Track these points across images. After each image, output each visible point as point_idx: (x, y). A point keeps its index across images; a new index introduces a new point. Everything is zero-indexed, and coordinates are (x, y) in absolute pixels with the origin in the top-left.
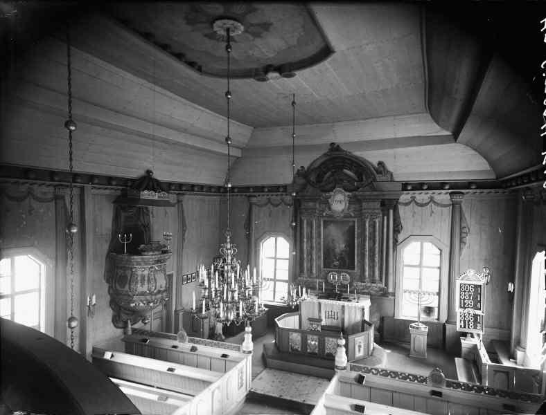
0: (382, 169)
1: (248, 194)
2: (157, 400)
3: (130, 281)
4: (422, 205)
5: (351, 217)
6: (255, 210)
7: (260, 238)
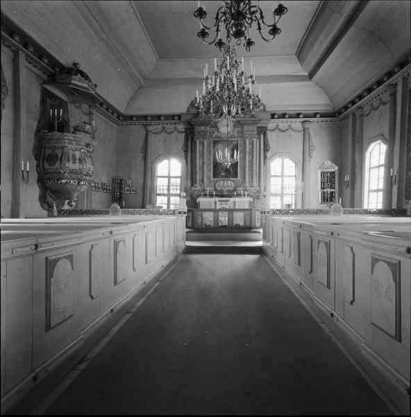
3: (61, 158)
4: (283, 131)
5: (235, 137)
6: (152, 137)
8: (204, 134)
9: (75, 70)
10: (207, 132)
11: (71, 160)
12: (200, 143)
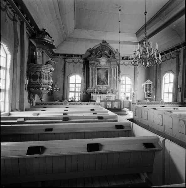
0: (117, 52)
3: (40, 77)
5: (107, 67)
6: (67, 64)
7: (164, 74)
9: (44, 33)
11: (45, 78)
12: (91, 69)
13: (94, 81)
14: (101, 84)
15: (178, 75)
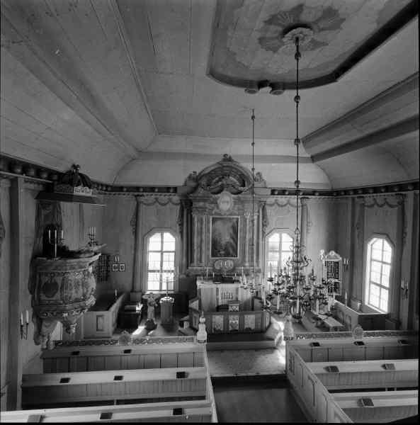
0: (259, 178)
1: (136, 194)
2: (172, 415)
5: (235, 215)
6: (142, 207)
7: (370, 238)
8: (203, 210)
10: (206, 208)
13: (204, 249)
14: (221, 255)
15: (402, 251)
